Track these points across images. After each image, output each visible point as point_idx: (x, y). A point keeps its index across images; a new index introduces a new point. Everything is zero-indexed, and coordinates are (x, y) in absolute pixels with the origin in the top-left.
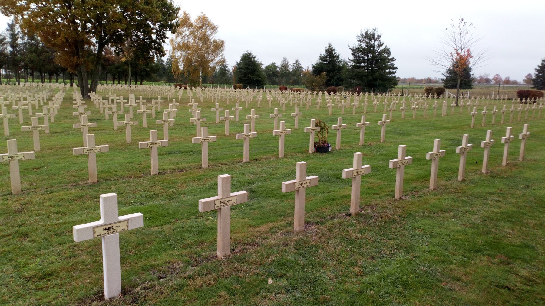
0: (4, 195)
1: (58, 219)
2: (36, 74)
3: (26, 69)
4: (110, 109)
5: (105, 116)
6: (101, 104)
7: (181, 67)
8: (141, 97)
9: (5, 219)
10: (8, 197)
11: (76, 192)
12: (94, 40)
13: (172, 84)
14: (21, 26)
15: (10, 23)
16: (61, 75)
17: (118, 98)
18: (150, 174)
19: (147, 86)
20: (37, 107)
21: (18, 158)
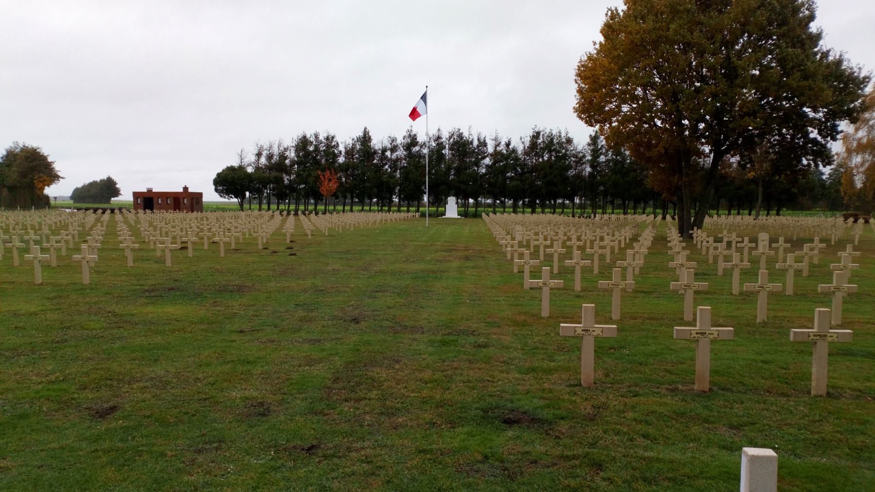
0: (570, 386)
1: (646, 449)
2: (619, 202)
3: (605, 196)
4: (727, 259)
5: (716, 269)
6: (704, 243)
7: (859, 182)
8: (781, 239)
9: (571, 427)
10: (576, 389)
11: (673, 402)
12: (707, 149)
13: (838, 213)
14: (607, 139)
15: (593, 134)
16: (651, 202)
17: (740, 239)
18: (809, 392)
19: (789, 218)
20: (616, 251)
21: (595, 334)
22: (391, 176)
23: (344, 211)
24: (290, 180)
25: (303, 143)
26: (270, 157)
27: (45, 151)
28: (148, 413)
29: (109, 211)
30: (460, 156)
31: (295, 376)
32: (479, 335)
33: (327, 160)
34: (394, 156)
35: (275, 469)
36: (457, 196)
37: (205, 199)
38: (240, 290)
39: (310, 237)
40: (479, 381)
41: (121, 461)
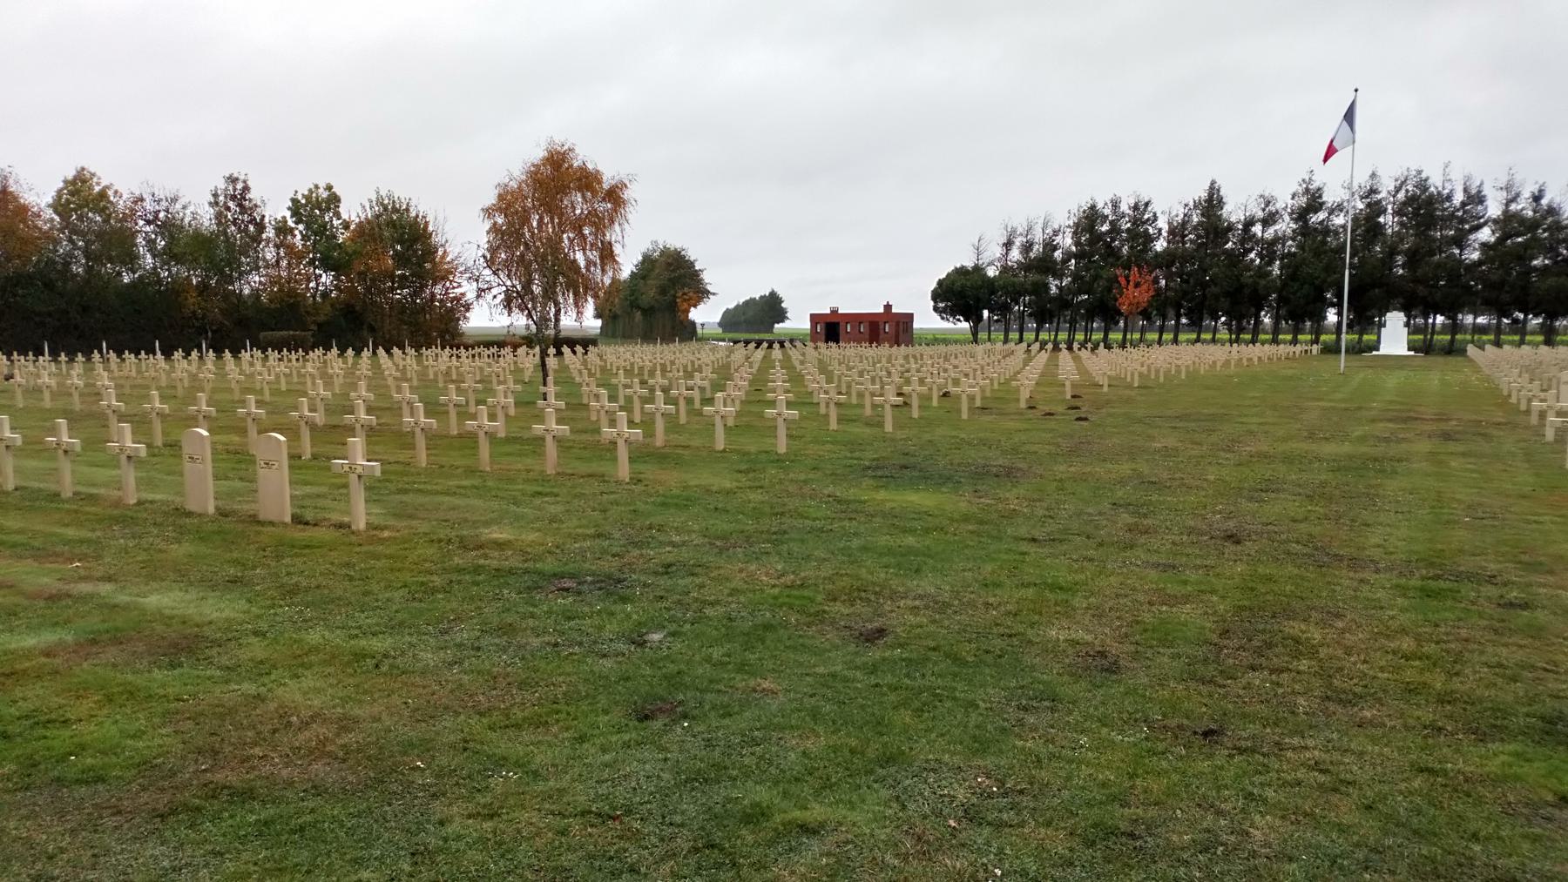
22: (1262, 273)
23: (1160, 342)
24: (1060, 288)
25: (1091, 217)
26: (1027, 247)
27: (692, 255)
28: (932, 644)
29: (776, 346)
30: (1418, 225)
31: (1147, 617)
32: (1505, 584)
33: (1131, 248)
34: (1270, 233)
35: (1152, 752)
36: (1407, 309)
38: (1009, 474)
39: (1106, 389)
40: (1523, 668)
41: (917, 704)
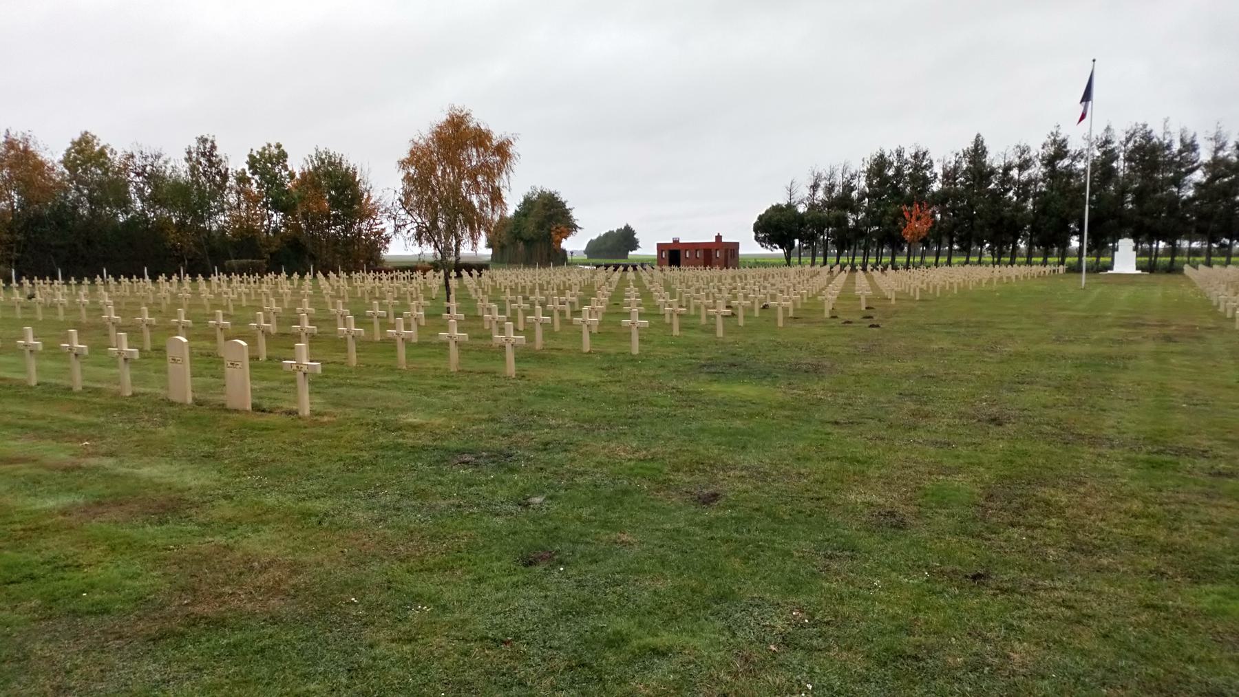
22: (1018, 207)
23: (936, 264)
24: (856, 221)
25: (880, 164)
26: (830, 189)
27: (563, 197)
29: (630, 269)
31: (927, 484)
32: (1215, 457)
33: (913, 188)
34: (1025, 176)
36: (1135, 236)
37: (742, 251)
38: (816, 371)
